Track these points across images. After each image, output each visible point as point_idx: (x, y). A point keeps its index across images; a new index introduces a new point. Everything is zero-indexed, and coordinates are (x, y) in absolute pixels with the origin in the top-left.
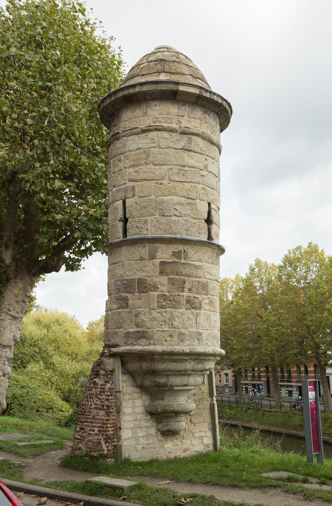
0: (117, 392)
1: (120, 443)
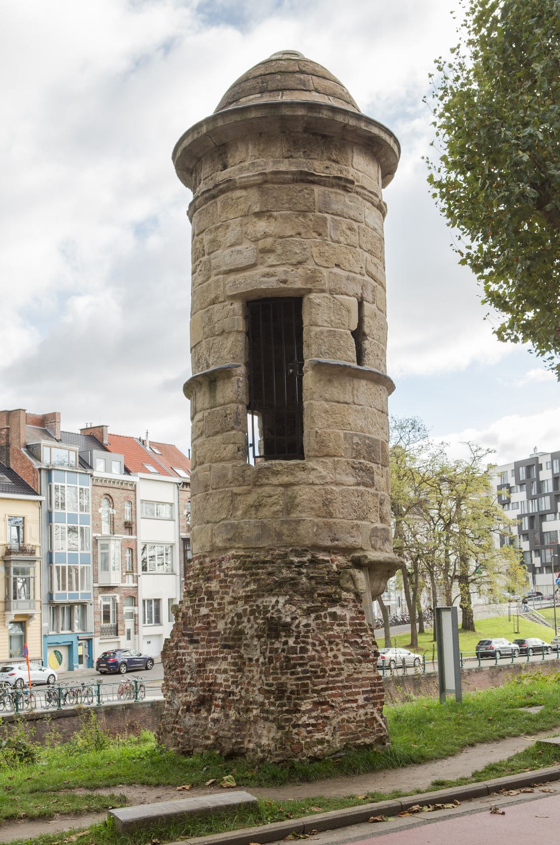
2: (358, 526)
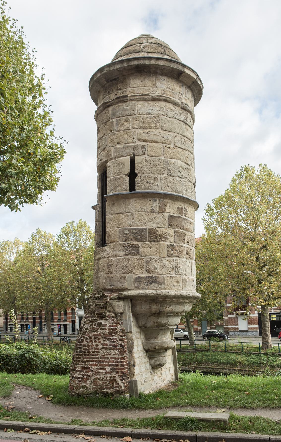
0: (127, 332)
1: (133, 379)
2: (124, 277)
